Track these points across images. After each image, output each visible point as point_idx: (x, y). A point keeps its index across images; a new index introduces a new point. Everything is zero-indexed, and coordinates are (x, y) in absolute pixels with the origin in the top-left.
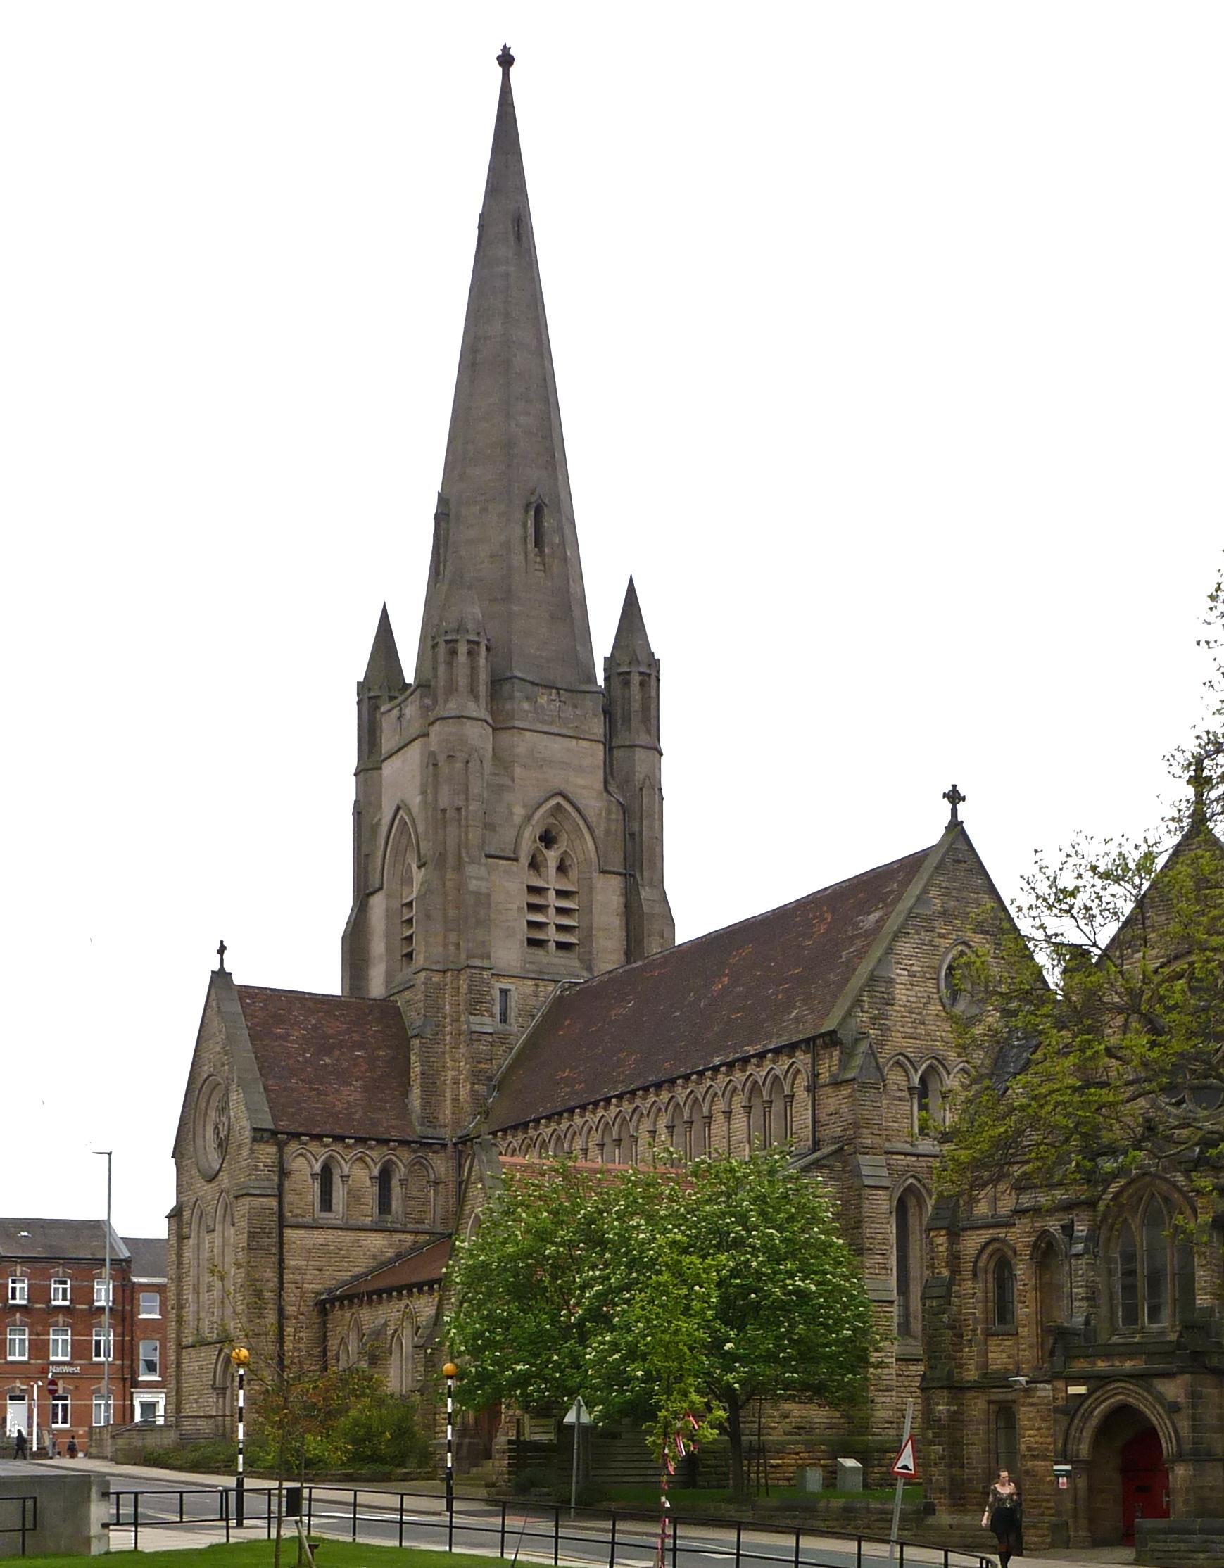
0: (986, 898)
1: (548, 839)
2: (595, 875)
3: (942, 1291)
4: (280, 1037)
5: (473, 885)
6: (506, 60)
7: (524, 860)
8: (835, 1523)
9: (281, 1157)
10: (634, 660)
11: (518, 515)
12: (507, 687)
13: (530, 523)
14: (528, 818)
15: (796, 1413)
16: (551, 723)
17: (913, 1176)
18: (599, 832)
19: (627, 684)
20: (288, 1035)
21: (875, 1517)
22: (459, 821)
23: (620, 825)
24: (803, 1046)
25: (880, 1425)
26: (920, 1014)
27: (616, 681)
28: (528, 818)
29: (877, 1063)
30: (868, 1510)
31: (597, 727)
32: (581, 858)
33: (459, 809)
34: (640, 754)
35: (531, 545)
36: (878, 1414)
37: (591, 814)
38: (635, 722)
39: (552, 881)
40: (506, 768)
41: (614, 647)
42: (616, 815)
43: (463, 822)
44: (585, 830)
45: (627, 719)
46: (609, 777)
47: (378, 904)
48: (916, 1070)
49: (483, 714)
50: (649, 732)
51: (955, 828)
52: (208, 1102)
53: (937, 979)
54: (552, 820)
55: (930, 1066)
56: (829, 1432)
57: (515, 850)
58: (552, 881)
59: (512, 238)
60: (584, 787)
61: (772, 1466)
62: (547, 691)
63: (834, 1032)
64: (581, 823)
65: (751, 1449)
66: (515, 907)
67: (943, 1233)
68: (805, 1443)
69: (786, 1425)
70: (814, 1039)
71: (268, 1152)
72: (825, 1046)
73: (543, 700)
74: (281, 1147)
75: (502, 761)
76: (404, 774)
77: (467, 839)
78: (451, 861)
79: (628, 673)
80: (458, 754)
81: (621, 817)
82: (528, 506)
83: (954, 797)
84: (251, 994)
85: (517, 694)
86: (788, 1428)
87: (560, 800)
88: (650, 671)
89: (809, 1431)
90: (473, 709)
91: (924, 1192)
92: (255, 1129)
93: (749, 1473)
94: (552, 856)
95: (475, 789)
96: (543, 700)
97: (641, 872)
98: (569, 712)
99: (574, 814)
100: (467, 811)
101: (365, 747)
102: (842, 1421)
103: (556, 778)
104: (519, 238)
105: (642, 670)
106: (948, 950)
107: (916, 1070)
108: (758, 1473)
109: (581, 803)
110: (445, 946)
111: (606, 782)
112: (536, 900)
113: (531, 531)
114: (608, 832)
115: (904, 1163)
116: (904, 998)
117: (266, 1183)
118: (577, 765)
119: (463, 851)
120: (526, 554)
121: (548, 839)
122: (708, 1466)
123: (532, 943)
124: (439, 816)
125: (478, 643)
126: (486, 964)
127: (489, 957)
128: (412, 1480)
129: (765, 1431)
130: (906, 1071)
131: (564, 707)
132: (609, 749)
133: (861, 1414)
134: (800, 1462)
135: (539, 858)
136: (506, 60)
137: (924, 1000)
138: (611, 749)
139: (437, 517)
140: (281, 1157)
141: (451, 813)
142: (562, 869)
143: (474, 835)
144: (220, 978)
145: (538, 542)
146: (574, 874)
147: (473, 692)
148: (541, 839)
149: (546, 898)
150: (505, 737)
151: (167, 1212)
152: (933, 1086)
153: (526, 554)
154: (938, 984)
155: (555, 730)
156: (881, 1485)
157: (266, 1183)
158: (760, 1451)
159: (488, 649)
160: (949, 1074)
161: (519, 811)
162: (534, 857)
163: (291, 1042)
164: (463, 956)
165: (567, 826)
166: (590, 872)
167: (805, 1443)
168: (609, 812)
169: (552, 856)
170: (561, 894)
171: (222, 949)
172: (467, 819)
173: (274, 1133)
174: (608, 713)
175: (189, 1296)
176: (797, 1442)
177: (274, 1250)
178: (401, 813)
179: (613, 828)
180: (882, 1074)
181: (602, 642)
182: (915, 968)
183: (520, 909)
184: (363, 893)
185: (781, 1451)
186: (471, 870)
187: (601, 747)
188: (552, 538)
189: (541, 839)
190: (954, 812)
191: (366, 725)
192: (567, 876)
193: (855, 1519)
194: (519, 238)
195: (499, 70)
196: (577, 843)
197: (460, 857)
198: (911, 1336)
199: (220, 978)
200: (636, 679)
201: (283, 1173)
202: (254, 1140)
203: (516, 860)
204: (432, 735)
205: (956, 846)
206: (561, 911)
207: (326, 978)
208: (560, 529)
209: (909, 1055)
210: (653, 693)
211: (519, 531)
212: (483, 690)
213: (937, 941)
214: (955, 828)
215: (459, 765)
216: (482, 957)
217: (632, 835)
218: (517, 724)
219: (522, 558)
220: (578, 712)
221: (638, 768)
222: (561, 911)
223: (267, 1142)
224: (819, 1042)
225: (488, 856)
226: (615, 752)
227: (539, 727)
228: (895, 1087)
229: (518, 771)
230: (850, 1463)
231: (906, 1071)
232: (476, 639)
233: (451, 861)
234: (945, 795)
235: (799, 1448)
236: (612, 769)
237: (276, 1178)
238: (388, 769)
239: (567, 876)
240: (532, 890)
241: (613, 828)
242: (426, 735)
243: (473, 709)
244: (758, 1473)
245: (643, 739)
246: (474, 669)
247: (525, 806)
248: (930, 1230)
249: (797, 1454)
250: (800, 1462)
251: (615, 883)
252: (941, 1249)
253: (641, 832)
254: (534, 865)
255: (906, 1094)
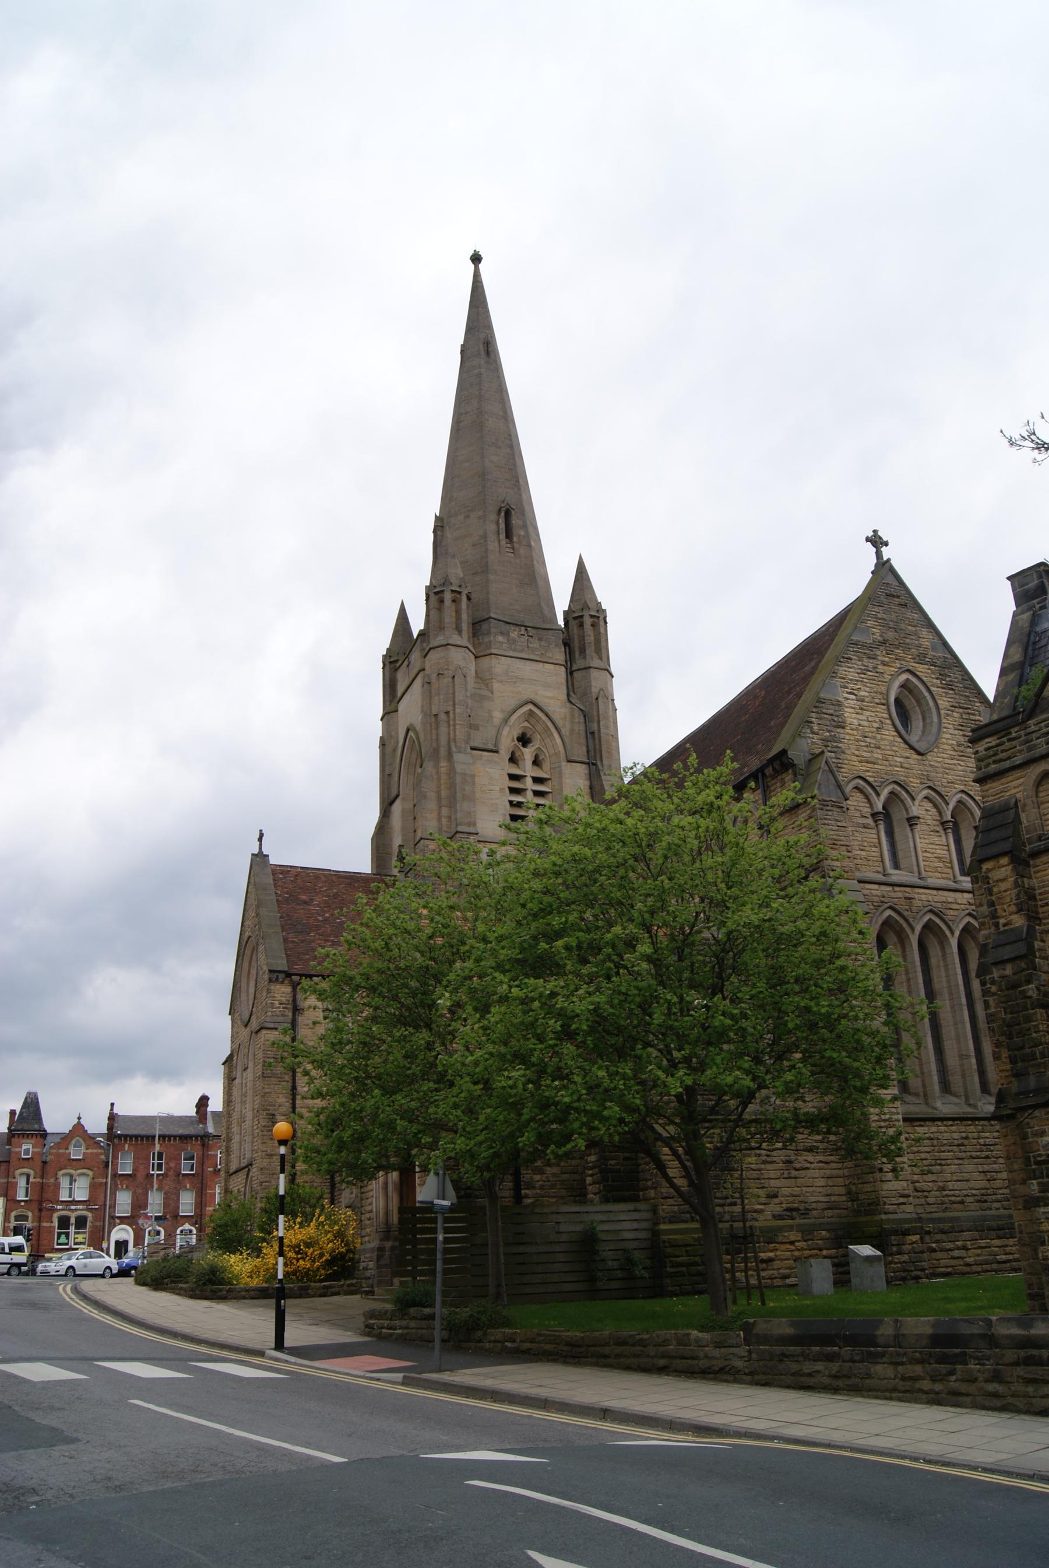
0: (924, 632)
1: (524, 740)
2: (564, 763)
3: (1021, 949)
4: (305, 902)
5: (459, 768)
6: (476, 259)
7: (505, 754)
8: (918, 1369)
9: (294, 996)
10: (585, 607)
11: (493, 517)
12: (485, 626)
13: (502, 521)
14: (506, 721)
15: (786, 1191)
16: (522, 651)
17: (890, 908)
18: (565, 731)
19: (581, 625)
20: (312, 900)
21: (1010, 1355)
22: (448, 722)
23: (582, 727)
24: (753, 784)
25: (894, 1201)
26: (874, 738)
27: (573, 624)
28: (506, 721)
29: (837, 781)
30: (992, 1341)
31: (560, 655)
32: (552, 751)
33: (447, 713)
34: (594, 674)
35: (503, 536)
36: (886, 1186)
37: (556, 717)
38: (590, 651)
39: (528, 770)
40: (487, 685)
41: (571, 601)
42: (579, 718)
43: (451, 722)
44: (553, 729)
45: (583, 651)
46: (571, 693)
47: (397, 808)
48: (878, 794)
49: (464, 642)
50: (601, 658)
51: (884, 569)
52: (250, 963)
53: (887, 705)
54: (526, 724)
55: (892, 793)
56: (830, 1213)
57: (495, 745)
58: (528, 770)
59: (483, 353)
60: (552, 698)
61: (763, 1261)
62: (517, 628)
63: (784, 752)
64: (549, 724)
65: (733, 1237)
66: (497, 788)
67: (1004, 861)
68: (801, 1229)
69: (774, 1207)
70: (761, 770)
71: (282, 991)
72: (777, 773)
73: (514, 635)
74: (295, 986)
75: (483, 679)
76: (411, 709)
77: (455, 736)
78: (443, 752)
79: (582, 617)
80: (446, 672)
81: (582, 720)
82: (499, 511)
83: (876, 541)
84: (284, 873)
85: (493, 630)
86: (778, 1209)
87: (531, 707)
88: (599, 618)
89: (806, 1213)
90: (456, 639)
91: (905, 925)
92: (271, 971)
93: (732, 1271)
94: (528, 753)
95: (460, 696)
96: (514, 635)
97: (601, 760)
98: (535, 644)
99: (544, 717)
100: (454, 714)
101: (387, 698)
102: (844, 1198)
103: (528, 692)
104: (488, 353)
105: (592, 613)
106: (894, 676)
107: (878, 794)
108: (746, 1270)
109: (549, 709)
110: (439, 819)
111: (568, 695)
112: (515, 785)
113: (502, 526)
114: (572, 731)
115: (879, 893)
116: (855, 722)
117: (281, 1019)
118: (544, 682)
119: (452, 744)
120: (499, 541)
121: (524, 740)
122: (680, 1265)
123: (514, 818)
124: (433, 719)
125: (460, 593)
126: (472, 830)
127: (475, 824)
128: (338, 1294)
129: (749, 1216)
130: (867, 797)
131: (531, 640)
132: (570, 673)
133: (868, 1188)
134: (796, 1253)
135: (517, 754)
136: (476, 259)
137: (876, 725)
138: (571, 673)
139: (435, 531)
140: (294, 996)
141: (443, 716)
142: (536, 762)
143: (461, 733)
144: (259, 859)
145: (509, 535)
146: (546, 766)
147: (459, 630)
148: (519, 739)
149: (525, 784)
150: (485, 662)
151: (224, 1059)
152: (898, 816)
153: (499, 541)
154: (888, 709)
155: (526, 656)
156: (904, 1279)
157: (281, 1019)
158: (743, 1241)
159: (469, 599)
160: (913, 799)
161: (498, 716)
162: (513, 753)
163: (314, 905)
164: (453, 825)
165: (539, 728)
166: (560, 762)
167: (801, 1229)
168: (573, 716)
169: (528, 753)
170: (537, 780)
171: (261, 836)
172: (454, 720)
173: (288, 975)
174: (566, 644)
175: (235, 1129)
176: (791, 1228)
177: (287, 1078)
178: (411, 733)
179: (577, 729)
180: (843, 793)
181: (561, 602)
182: (862, 693)
183: (502, 790)
184: (387, 803)
185: (771, 1237)
186: (458, 757)
187: (563, 669)
188: (518, 532)
189: (519, 739)
190: (879, 555)
191: (388, 682)
192: (541, 768)
193: (963, 1359)
194: (488, 353)
195: (471, 267)
196: (547, 741)
197: (450, 748)
198: (910, 1094)
199: (259, 859)
200: (588, 621)
201: (296, 1010)
202: (270, 981)
203: (497, 752)
204: (427, 668)
205: (887, 590)
206: (537, 793)
207: (362, 863)
208: (525, 527)
209: (871, 780)
210: (602, 631)
211: (494, 527)
212: (465, 626)
213: (881, 668)
214: (884, 569)
215: (447, 680)
216: (469, 824)
217: (593, 733)
218: (493, 651)
219: (496, 544)
220: (543, 643)
221: (593, 683)
222: (537, 793)
223: (282, 982)
224: (769, 771)
225: (473, 749)
226: (575, 674)
227: (511, 654)
228: (858, 814)
229: (496, 685)
230: (866, 1250)
231: (867, 797)
232: (458, 589)
233: (443, 752)
234: (868, 540)
235: (793, 1236)
236: (573, 685)
237: (290, 1014)
238: (402, 706)
239: (541, 768)
240: (513, 777)
241: (577, 729)
242: (424, 670)
243: (456, 639)
244: (746, 1270)
245: (596, 662)
246: (458, 612)
247: (502, 711)
248: (982, 861)
249: (792, 1243)
250: (796, 1253)
251: (582, 769)
252: (1003, 886)
253: (599, 731)
254: (513, 760)
255: (870, 821)
